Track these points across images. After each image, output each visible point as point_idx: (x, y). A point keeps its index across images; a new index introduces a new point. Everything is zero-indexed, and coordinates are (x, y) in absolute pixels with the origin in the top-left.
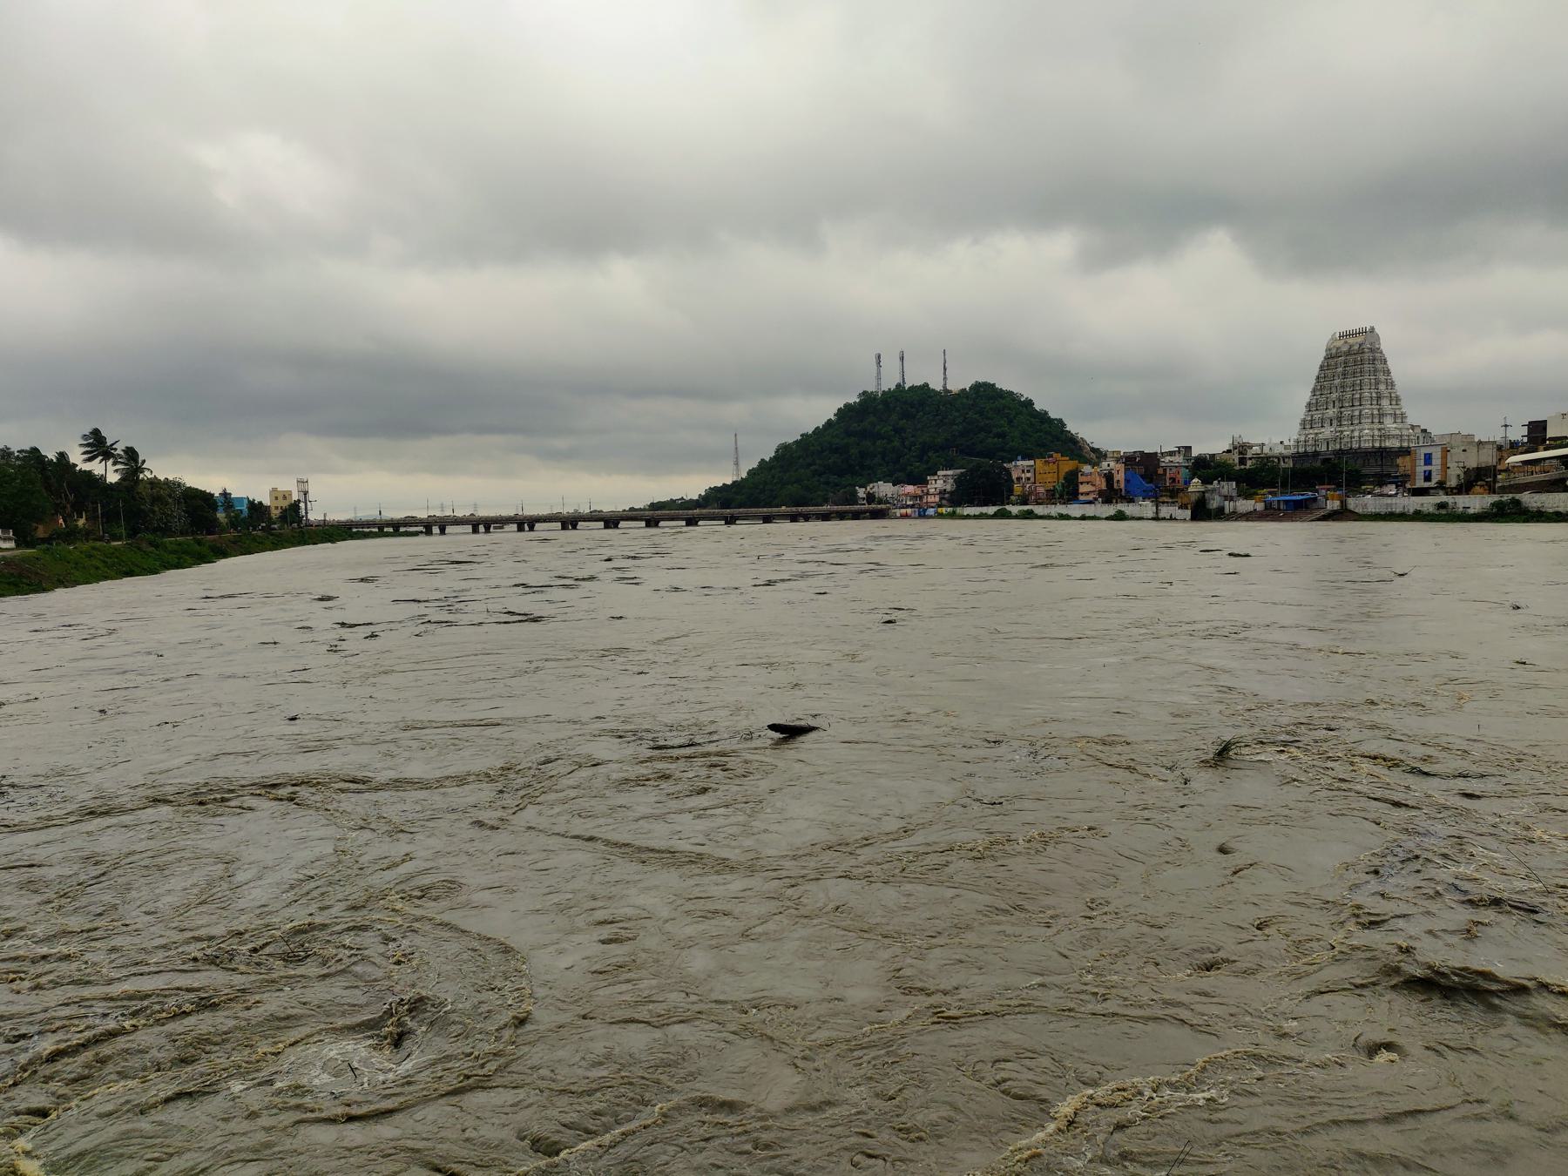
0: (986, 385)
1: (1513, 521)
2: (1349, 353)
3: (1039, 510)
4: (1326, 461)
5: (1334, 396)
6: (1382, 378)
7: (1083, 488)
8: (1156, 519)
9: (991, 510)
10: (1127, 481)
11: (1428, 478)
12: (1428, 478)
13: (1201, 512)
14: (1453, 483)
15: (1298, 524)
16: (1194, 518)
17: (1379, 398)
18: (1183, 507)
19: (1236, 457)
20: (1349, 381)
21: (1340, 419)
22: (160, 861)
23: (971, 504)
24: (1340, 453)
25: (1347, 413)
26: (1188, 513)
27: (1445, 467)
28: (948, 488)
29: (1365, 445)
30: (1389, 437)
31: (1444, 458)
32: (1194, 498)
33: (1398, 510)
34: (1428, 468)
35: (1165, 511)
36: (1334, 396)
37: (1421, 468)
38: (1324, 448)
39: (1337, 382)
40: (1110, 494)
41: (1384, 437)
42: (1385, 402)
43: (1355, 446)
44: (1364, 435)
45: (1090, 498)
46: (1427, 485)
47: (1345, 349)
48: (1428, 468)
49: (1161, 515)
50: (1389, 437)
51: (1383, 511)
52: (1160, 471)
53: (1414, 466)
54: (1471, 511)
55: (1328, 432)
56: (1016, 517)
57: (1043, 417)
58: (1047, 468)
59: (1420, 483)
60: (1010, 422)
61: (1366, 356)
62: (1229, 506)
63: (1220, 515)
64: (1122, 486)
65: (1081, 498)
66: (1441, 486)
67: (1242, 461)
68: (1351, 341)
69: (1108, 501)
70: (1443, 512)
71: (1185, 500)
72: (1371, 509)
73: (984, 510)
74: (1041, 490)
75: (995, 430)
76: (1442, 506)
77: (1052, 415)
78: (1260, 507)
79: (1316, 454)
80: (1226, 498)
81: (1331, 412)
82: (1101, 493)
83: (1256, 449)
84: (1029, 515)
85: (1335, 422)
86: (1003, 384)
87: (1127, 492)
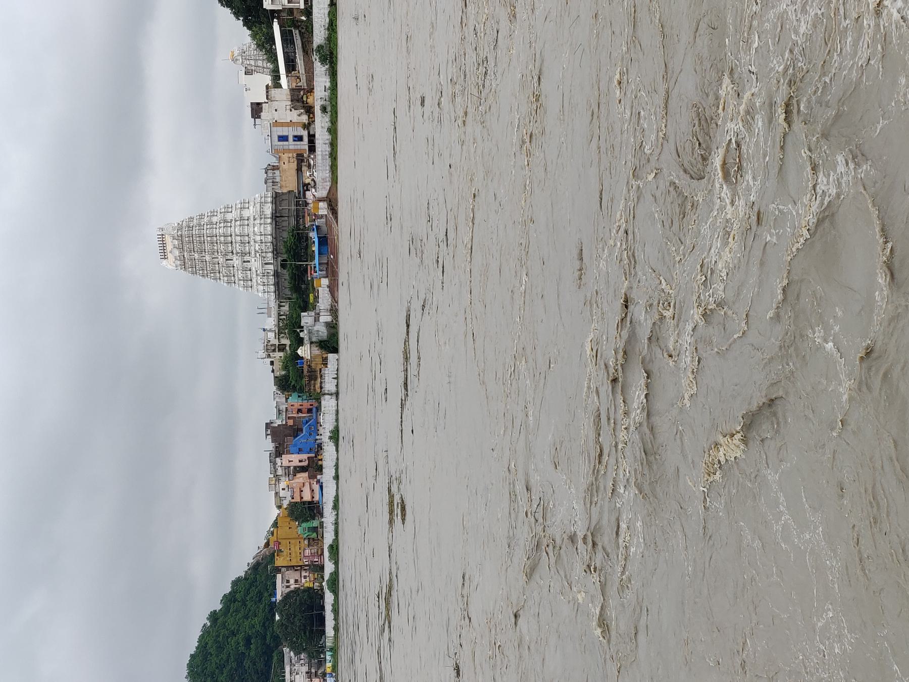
0: (190, 666)
1: (336, 45)
2: (181, 249)
3: (329, 538)
4: (283, 266)
5: (221, 260)
6: (206, 219)
7: (307, 497)
8: (337, 394)
9: (329, 598)
10: (300, 451)
11: (299, 138)
12: (299, 138)
13: (330, 345)
14: (304, 119)
15: (339, 56)
16: (335, 350)
17: (225, 221)
18: (325, 362)
19: (279, 355)
20: (207, 247)
21: (243, 254)
22: (638, 380)
23: (322, 620)
24: (276, 252)
25: (238, 248)
26: (331, 357)
27: (291, 124)
28: (305, 669)
29: (269, 229)
30: (262, 212)
31: (283, 125)
32: (317, 351)
33: (328, 149)
34: (291, 138)
35: (329, 386)
36: (221, 260)
37: (291, 144)
38: (271, 267)
39: (208, 258)
40: (314, 468)
41: (262, 215)
42: (229, 217)
43: (269, 238)
44: (261, 233)
45: (316, 487)
46: (306, 139)
47: (177, 252)
48: (291, 138)
49: (334, 389)
50: (262, 212)
51: (328, 162)
52: (291, 422)
53: (289, 151)
54: (328, 85)
55: (255, 264)
56: (336, 563)
57: (229, 600)
58: (286, 552)
59: (304, 145)
60: (233, 634)
61: (185, 233)
62: (325, 318)
63: (333, 327)
64: (305, 456)
65: (317, 498)
66: (306, 126)
67: (282, 348)
68: (169, 247)
69: (320, 469)
70: (329, 109)
71: (319, 360)
72: (327, 174)
73: (328, 608)
74: (307, 552)
75: (242, 649)
76: (324, 109)
77: (228, 589)
78: (325, 282)
79: (276, 274)
80: (317, 319)
81: (236, 261)
82: (312, 477)
83: (271, 335)
84: (334, 549)
85: (246, 258)
86: (192, 646)
87: (310, 451)
